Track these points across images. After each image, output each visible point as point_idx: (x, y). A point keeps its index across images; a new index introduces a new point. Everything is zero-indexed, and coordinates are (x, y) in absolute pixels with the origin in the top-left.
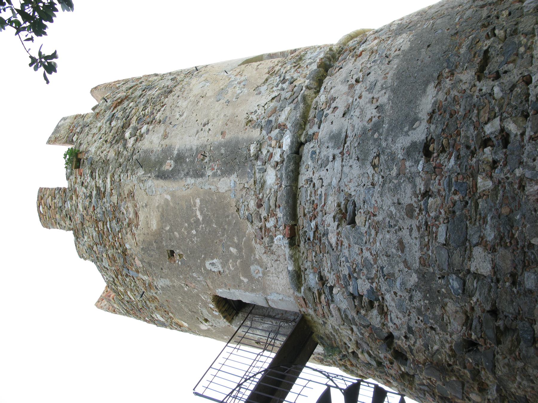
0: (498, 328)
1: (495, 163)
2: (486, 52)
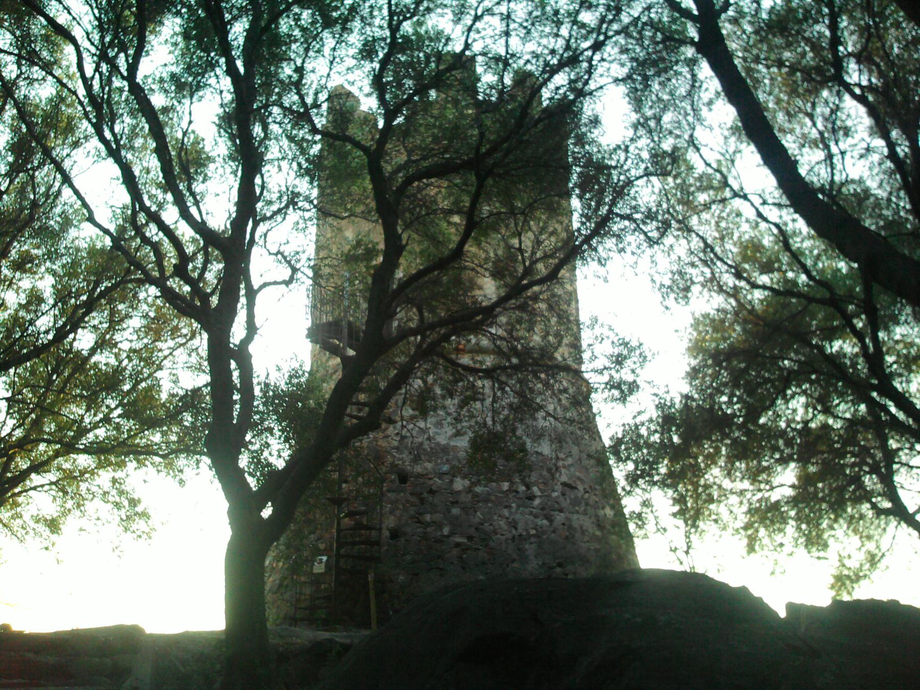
0: (422, 494)
1: (517, 492)
2: (576, 488)
